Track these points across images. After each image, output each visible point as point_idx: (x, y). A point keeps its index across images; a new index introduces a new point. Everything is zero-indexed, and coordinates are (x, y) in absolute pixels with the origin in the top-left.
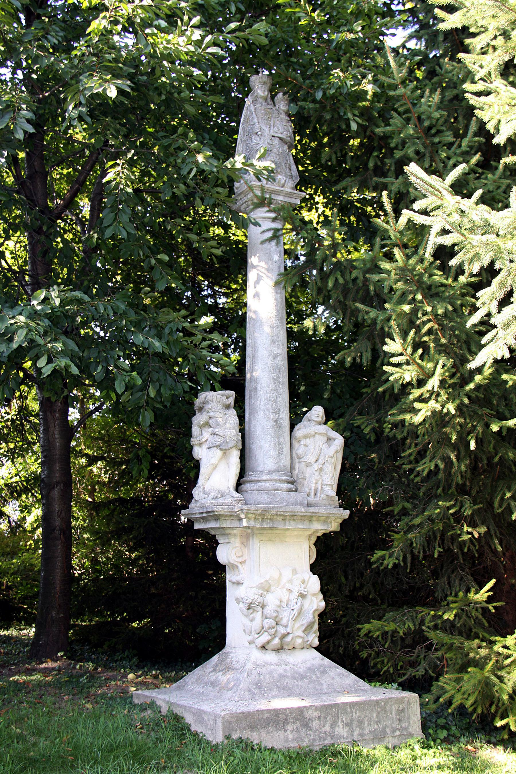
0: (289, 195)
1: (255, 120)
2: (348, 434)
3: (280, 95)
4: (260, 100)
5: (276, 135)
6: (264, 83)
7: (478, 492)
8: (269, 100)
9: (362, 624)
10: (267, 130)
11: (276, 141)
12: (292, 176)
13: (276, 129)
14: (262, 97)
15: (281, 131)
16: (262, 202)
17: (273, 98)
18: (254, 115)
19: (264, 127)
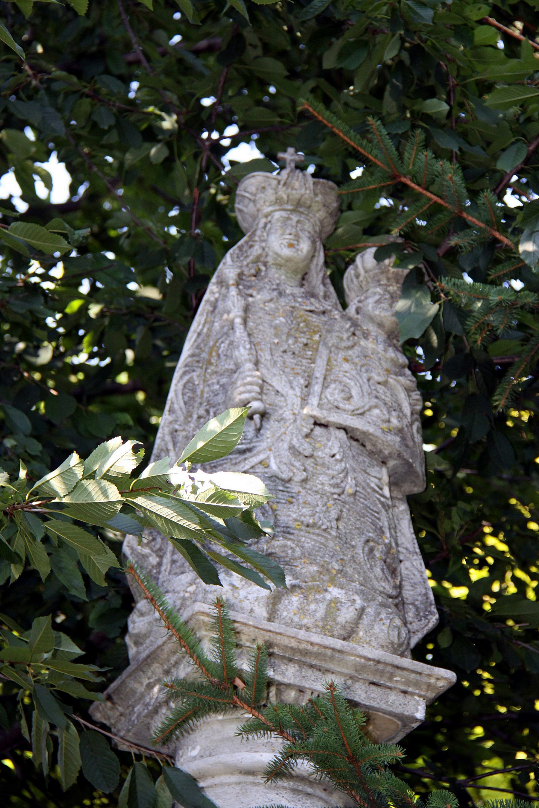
0: (377, 675)
1: (243, 353)
2: (118, 641)
3: (366, 259)
4: (276, 275)
5: (334, 418)
6: (299, 206)
7: (235, 687)
8: (318, 273)
9: (40, 478)
10: (293, 396)
11: (334, 443)
12: (398, 602)
13: (333, 394)
14: (282, 264)
15: (357, 401)
16: (220, 690)
17: (337, 266)
18: (240, 332)
19: (278, 382)
